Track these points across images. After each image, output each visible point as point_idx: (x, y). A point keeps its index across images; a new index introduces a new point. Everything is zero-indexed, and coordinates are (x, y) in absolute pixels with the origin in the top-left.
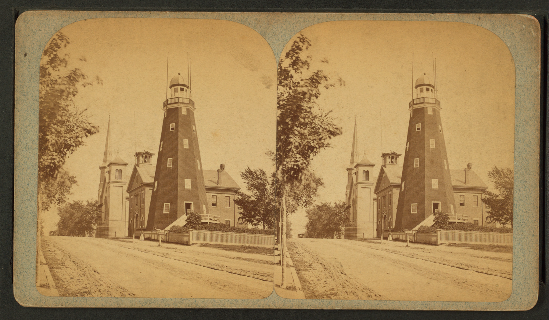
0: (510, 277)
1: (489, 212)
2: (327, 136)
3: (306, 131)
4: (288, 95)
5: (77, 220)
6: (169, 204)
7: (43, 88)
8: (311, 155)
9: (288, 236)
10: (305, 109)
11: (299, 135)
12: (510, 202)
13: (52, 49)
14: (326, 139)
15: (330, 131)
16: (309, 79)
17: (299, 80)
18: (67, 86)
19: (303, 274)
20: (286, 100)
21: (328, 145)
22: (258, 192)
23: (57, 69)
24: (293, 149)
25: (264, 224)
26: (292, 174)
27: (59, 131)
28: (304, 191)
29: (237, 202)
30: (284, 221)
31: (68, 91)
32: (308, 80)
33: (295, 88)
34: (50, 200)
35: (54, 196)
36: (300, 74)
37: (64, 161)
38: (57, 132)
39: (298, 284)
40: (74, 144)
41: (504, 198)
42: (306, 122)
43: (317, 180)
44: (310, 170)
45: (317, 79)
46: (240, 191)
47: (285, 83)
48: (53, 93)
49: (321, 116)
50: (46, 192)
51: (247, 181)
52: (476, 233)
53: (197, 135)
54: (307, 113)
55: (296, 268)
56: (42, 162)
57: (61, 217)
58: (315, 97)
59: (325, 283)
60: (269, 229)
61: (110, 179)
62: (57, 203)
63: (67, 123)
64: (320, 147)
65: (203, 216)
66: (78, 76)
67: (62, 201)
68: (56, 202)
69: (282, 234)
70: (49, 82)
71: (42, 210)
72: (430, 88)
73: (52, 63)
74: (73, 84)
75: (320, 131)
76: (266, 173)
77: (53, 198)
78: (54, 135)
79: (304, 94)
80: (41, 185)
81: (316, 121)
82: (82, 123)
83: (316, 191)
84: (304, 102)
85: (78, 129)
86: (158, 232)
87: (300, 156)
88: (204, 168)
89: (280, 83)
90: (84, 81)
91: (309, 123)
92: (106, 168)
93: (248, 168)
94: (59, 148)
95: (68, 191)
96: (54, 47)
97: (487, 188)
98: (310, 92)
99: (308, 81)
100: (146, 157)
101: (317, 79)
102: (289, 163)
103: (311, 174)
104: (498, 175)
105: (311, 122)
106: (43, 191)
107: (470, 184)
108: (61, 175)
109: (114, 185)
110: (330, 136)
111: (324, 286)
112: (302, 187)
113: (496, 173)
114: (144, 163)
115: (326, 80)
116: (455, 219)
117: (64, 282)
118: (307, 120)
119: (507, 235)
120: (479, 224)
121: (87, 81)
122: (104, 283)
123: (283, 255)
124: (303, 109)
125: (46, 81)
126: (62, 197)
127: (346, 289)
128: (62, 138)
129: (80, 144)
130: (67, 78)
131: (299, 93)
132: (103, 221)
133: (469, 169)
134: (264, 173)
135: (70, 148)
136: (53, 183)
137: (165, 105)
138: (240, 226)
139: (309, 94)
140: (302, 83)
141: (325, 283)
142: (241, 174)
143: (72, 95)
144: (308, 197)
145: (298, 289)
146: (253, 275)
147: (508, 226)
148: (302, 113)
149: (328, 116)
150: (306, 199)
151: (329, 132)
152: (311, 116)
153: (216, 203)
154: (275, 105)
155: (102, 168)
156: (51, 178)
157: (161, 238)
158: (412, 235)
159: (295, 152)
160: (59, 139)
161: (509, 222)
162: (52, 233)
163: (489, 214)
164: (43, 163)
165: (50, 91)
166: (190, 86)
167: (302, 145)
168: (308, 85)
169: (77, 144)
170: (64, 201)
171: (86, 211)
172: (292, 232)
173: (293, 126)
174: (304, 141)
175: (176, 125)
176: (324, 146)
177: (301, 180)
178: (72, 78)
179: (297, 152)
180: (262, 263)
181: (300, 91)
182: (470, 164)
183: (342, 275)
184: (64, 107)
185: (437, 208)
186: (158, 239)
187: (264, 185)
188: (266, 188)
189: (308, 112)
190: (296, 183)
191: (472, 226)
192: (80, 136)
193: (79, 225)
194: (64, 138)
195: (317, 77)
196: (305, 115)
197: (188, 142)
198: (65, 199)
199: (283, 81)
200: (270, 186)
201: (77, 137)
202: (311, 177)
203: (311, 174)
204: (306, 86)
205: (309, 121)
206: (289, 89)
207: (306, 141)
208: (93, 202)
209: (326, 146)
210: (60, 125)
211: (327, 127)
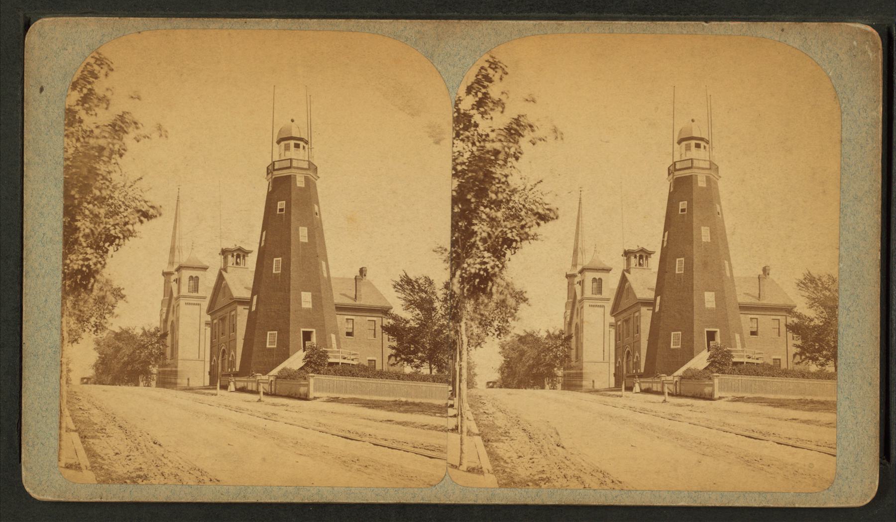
0: (832, 451)
3: (499, 214)
4: (470, 155)
5: (126, 359)
6: (276, 332)
7: (70, 143)
8: (508, 252)
9: (471, 384)
10: (498, 178)
11: (488, 220)
12: (832, 330)
13: (85, 80)
14: (532, 226)
15: (538, 213)
16: (505, 128)
18: (109, 140)
21: (535, 237)
22: (421, 313)
23: (93, 113)
24: (478, 242)
25: (430, 366)
26: (476, 283)
27: (96, 214)
28: (495, 312)
29: (387, 329)
30: (463, 360)
31: (111, 149)
32: (502, 130)
33: (482, 144)
35: (88, 319)
36: (489, 121)
37: (105, 263)
38: (93, 215)
39: (486, 464)
42: (499, 199)
43: (517, 293)
44: (506, 278)
45: (518, 128)
47: (464, 136)
48: (87, 152)
49: (524, 189)
52: (777, 381)
54: (501, 185)
55: (483, 437)
56: (69, 264)
57: (99, 354)
58: (514, 159)
59: (531, 461)
62: (92, 332)
63: (110, 200)
64: (521, 240)
65: (332, 352)
66: (127, 125)
67: (101, 328)
68: (91, 330)
69: (460, 381)
70: (80, 133)
71: (69, 342)
73: (86, 103)
74: (119, 137)
75: (523, 213)
76: (435, 282)
77: (86, 323)
79: (496, 153)
80: (67, 301)
81: (516, 198)
82: (133, 201)
83: (516, 312)
84: (496, 166)
85: (127, 210)
86: (258, 378)
87: (490, 255)
88: (333, 274)
89: (458, 135)
90: (138, 132)
91: (504, 200)
93: (404, 274)
94: (96, 241)
95: (110, 312)
96: (88, 76)
97: (795, 307)
98: (507, 149)
99: (502, 133)
100: (238, 256)
101: (518, 128)
102: (472, 265)
103: (508, 285)
104: (812, 286)
105: (507, 200)
106: (70, 312)
107: (766, 301)
108: (99, 285)
109: (187, 302)
110: (538, 221)
111: (529, 466)
112: (492, 305)
113: (810, 282)
114: (235, 265)
115: (533, 131)
116: (742, 357)
117: (104, 460)
118: (500, 196)
120: (782, 366)
121: (142, 132)
122: (170, 461)
123: (462, 417)
124: (494, 178)
125: (75, 132)
126: (102, 321)
127: (564, 472)
128: (101, 225)
129: (130, 234)
130: (110, 127)
131: (488, 152)
132: (168, 361)
134: (431, 283)
135: (114, 241)
136: (86, 298)
138: (392, 369)
140: (492, 136)
142: (394, 283)
143: (118, 155)
144: (503, 321)
145: (487, 471)
146: (413, 449)
147: (830, 368)
149: (535, 190)
150: (499, 324)
151: (537, 216)
152: (507, 190)
154: (450, 172)
155: (166, 274)
157: (263, 388)
159: (482, 248)
161: (831, 363)
162: (85, 380)
163: (799, 349)
164: (71, 265)
165: (81, 149)
166: (309, 141)
167: (493, 236)
168: (503, 139)
169: (126, 235)
170: (104, 328)
172: (476, 379)
173: (479, 206)
174: (496, 229)
176: (530, 238)
177: (491, 294)
178: (117, 128)
179: (485, 247)
180: (428, 429)
181: (490, 149)
182: (767, 268)
184: (104, 174)
185: (713, 339)
187: (431, 302)
188: (435, 306)
189: (503, 183)
190: (483, 298)
191: (771, 368)
192: (131, 222)
193: (129, 368)
194: (104, 225)
195: (517, 125)
196: (498, 188)
198: (106, 325)
199: (461, 132)
200: (441, 303)
201: (126, 224)
203: (508, 285)
204: (500, 140)
205: (504, 198)
206: (472, 146)
207: (500, 229)
208: (152, 330)
209: (533, 239)
211: (534, 207)
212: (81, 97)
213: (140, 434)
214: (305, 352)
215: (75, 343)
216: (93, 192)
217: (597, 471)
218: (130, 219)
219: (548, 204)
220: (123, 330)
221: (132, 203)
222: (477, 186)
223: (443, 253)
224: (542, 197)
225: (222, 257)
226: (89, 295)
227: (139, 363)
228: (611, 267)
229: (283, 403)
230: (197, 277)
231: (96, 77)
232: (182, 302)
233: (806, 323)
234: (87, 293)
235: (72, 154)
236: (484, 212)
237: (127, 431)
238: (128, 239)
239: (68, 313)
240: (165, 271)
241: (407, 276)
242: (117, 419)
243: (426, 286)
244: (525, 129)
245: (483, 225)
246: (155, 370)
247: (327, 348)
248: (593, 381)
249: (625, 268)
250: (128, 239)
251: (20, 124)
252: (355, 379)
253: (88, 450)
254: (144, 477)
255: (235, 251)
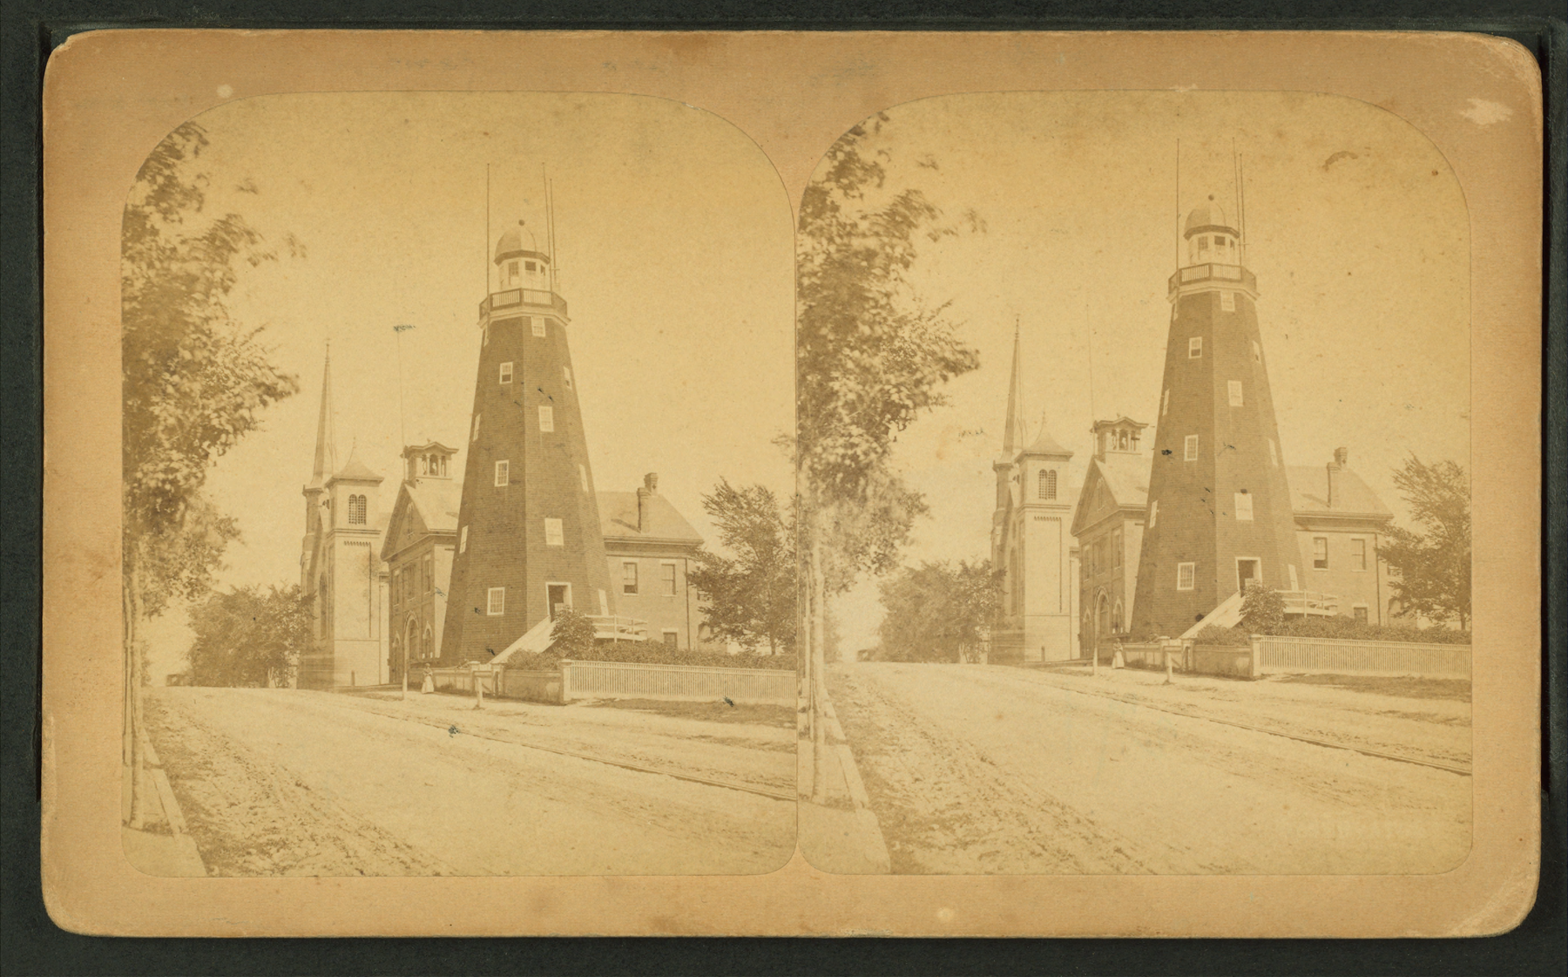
0: (1465, 768)
1: (1397, 586)
2: (938, 373)
3: (877, 361)
4: (826, 260)
5: (244, 640)
8: (893, 426)
9: (831, 656)
11: (857, 370)
12: (1455, 558)
13: (160, 162)
15: (943, 359)
17: (855, 217)
18: (205, 264)
19: (872, 762)
20: (820, 274)
21: (940, 401)
22: (753, 551)
23: (175, 217)
24: (840, 410)
25: (772, 640)
26: (838, 480)
27: (186, 393)
28: (872, 529)
29: (695, 579)
31: (208, 279)
32: (881, 216)
33: (846, 240)
34: (165, 586)
35: (177, 574)
36: (858, 200)
37: (204, 477)
38: (180, 393)
40: (229, 428)
41: (1439, 547)
42: (877, 335)
45: (907, 213)
46: (702, 548)
47: (815, 226)
49: (920, 318)
50: (154, 565)
51: (723, 521)
53: (575, 394)
54: (879, 310)
55: (853, 746)
56: (140, 480)
57: (198, 633)
58: (901, 265)
60: (787, 655)
61: (333, 522)
62: (185, 595)
63: (209, 368)
64: (916, 405)
65: (601, 620)
66: (235, 236)
67: (199, 588)
68: (182, 593)
69: (812, 651)
70: (154, 254)
71: (144, 614)
72: (1228, 237)
73: (164, 201)
74: (222, 259)
75: (917, 359)
76: (776, 495)
77: (173, 581)
78: (172, 402)
79: (870, 255)
80: (140, 543)
81: (905, 332)
82: (249, 368)
84: (871, 278)
85: (239, 383)
86: (474, 669)
87: (861, 431)
88: (600, 486)
89: (803, 225)
90: (253, 248)
91: (885, 337)
92: (322, 492)
93: (723, 484)
94: (186, 438)
95: (215, 560)
97: (1392, 518)
98: (888, 250)
99: (880, 220)
100: (433, 459)
101: (907, 213)
103: (892, 482)
104: (1420, 482)
105: (890, 336)
106: (144, 563)
108: (195, 515)
110: (945, 372)
111: (933, 795)
112: (865, 518)
113: (1416, 474)
114: (428, 475)
115: (933, 217)
116: (1301, 605)
117: (210, 815)
118: (878, 330)
119: (1451, 650)
120: (1369, 620)
123: (815, 712)
124: (867, 299)
125: (145, 250)
126: (201, 577)
127: (994, 806)
128: (195, 410)
129: (248, 424)
131: (856, 254)
133: (1340, 464)
134: (769, 498)
135: (218, 437)
136: (172, 537)
137: (483, 311)
138: (705, 647)
139: (884, 256)
140: (864, 226)
141: (937, 787)
142: (705, 499)
143: (220, 290)
144: (886, 546)
145: (861, 805)
146: (745, 785)
147: (1453, 624)
148: (864, 309)
149: (938, 318)
150: (879, 551)
151: (943, 363)
152: (890, 319)
153: (636, 585)
154: (792, 290)
155: (310, 493)
156: (166, 524)
158: (1179, 652)
159: (847, 420)
160: (187, 413)
162: (175, 679)
164: (144, 481)
165: (155, 280)
167: (867, 399)
168: (881, 230)
169: (237, 426)
170: (204, 590)
171: (268, 615)
172: (840, 646)
173: (841, 348)
174: (872, 387)
175: (515, 367)
176: (930, 401)
177: (865, 499)
178: (217, 243)
179: (852, 418)
180: (770, 749)
181: (858, 249)
182: (1342, 451)
183: (984, 765)
184: (198, 322)
185: (1251, 575)
186: (473, 687)
187: (770, 530)
188: (777, 537)
189: (882, 307)
190: (851, 505)
192: (247, 404)
193: (250, 656)
194: (201, 411)
195: (907, 208)
196: (874, 315)
197: (551, 413)
198: (209, 584)
199: (810, 220)
200: (787, 532)
201: (238, 406)
202: (893, 491)
204: (877, 234)
205: (885, 333)
206: (829, 244)
207: (877, 387)
208: (289, 590)
209: (935, 403)
210: (189, 376)
211: (935, 348)
212: (153, 191)
213: (272, 770)
214: (555, 622)
215: (155, 616)
216: (180, 355)
217: (1052, 803)
218: (244, 399)
219: (961, 343)
220: (238, 591)
221: (247, 372)
222: (839, 312)
223: (788, 446)
224: (951, 331)
225: (407, 461)
226: (176, 532)
227: (267, 647)
228: (1071, 450)
229: (519, 711)
230: (363, 497)
231: (179, 156)
232: (339, 541)
233: (1411, 547)
234: (174, 529)
235: (141, 290)
236: (850, 357)
237: (250, 766)
238: (243, 435)
239: (141, 564)
240: (306, 488)
241: (728, 487)
242: (232, 744)
243: (761, 503)
244: (920, 214)
245: (848, 379)
246: (294, 659)
247: (591, 613)
248: (1043, 649)
249: (1096, 453)
250: (243, 435)
251: (35, 213)
252: (642, 667)
253: (182, 799)
254: (282, 843)
255: (428, 449)
